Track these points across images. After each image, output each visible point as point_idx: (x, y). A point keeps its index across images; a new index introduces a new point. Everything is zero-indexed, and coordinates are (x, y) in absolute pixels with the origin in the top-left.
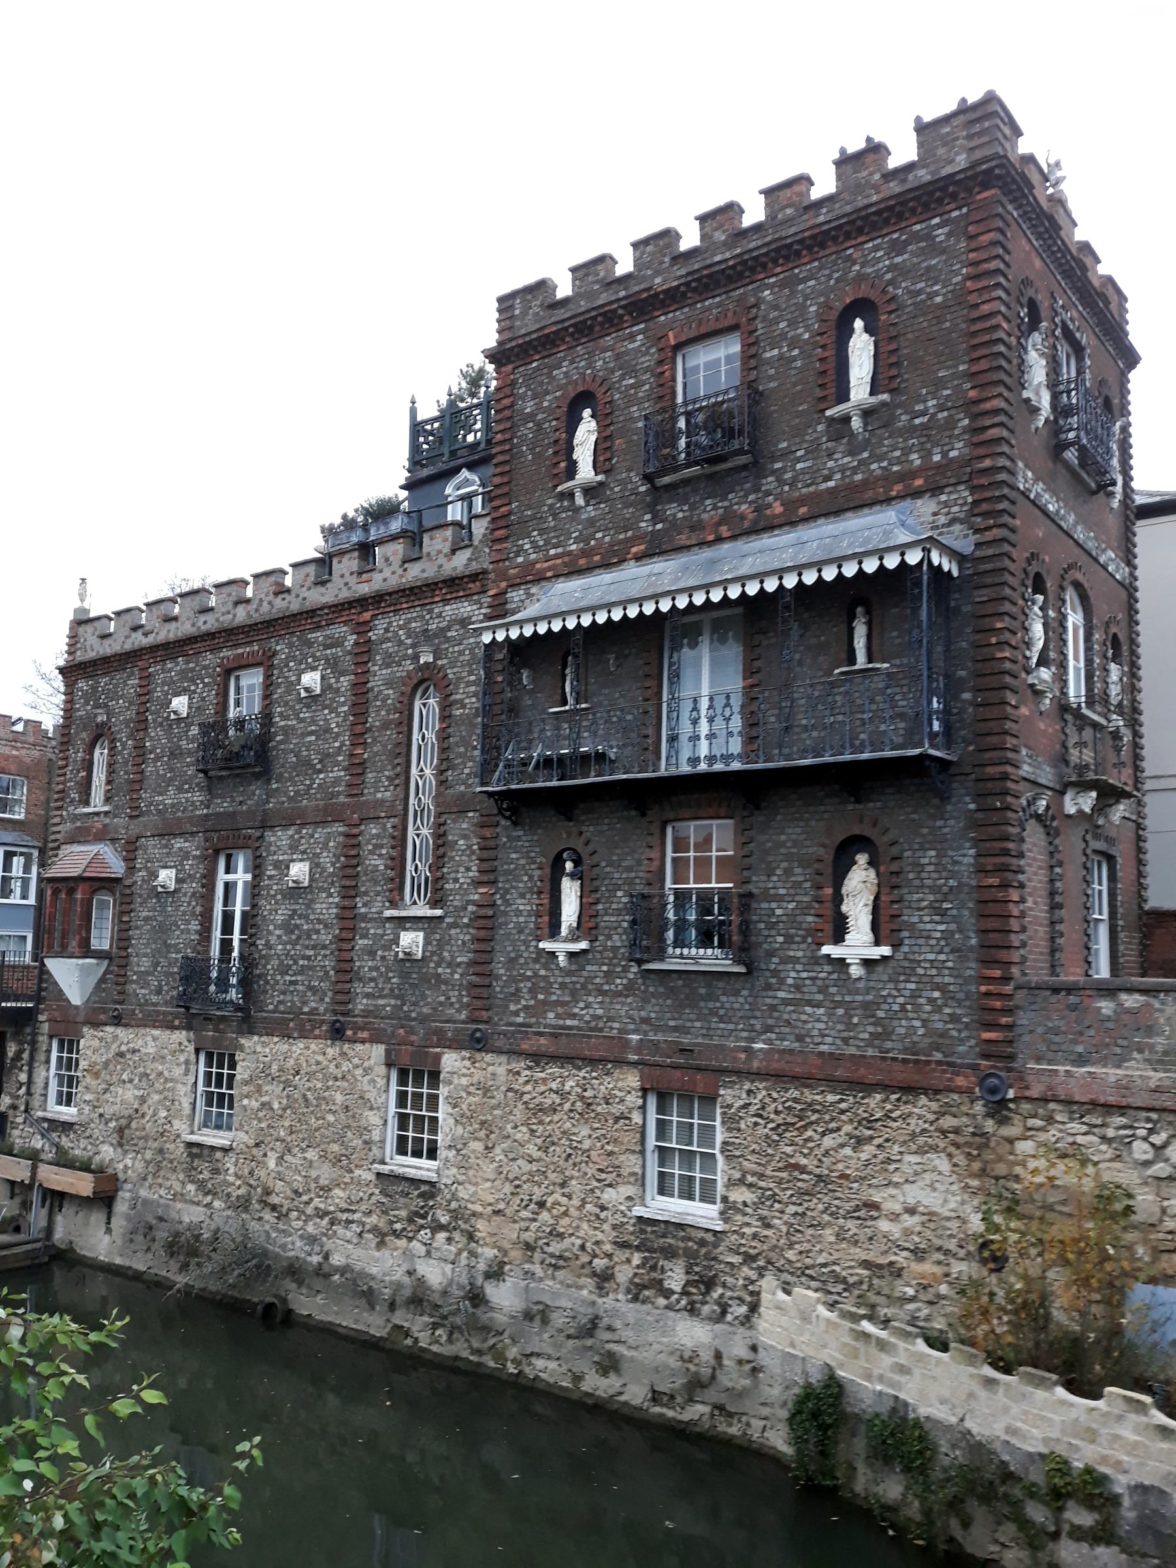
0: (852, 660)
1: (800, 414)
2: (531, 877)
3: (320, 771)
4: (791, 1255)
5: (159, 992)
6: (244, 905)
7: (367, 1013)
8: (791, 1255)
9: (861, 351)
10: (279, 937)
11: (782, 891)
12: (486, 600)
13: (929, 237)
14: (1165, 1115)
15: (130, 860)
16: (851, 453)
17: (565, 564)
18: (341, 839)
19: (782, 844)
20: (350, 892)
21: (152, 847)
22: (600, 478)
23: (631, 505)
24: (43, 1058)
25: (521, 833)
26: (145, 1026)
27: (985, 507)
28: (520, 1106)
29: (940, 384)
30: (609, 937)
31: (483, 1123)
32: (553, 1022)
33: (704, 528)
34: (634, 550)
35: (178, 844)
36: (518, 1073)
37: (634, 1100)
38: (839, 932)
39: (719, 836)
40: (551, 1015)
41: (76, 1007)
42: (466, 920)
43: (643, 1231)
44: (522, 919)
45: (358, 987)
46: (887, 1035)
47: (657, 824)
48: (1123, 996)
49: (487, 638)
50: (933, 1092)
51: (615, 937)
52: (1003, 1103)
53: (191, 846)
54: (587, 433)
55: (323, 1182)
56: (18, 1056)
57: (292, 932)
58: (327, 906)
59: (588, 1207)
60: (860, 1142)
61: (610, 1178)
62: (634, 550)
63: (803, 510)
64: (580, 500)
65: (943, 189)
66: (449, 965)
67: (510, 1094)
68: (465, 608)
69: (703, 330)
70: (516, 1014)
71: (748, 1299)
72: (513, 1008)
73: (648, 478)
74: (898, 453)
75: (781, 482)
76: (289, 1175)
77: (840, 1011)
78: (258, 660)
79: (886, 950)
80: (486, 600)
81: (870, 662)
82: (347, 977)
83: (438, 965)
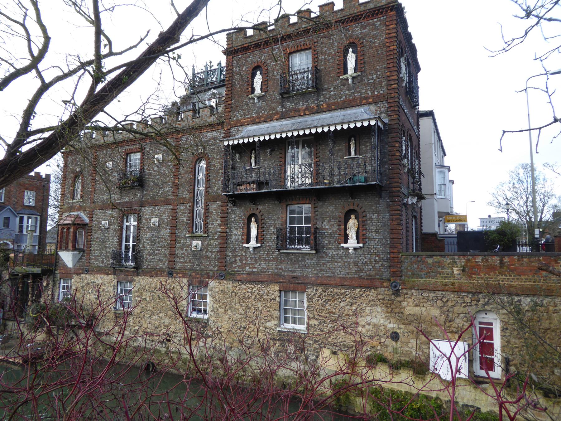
0: (350, 154)
1: (331, 77)
2: (240, 223)
3: (162, 188)
4: (330, 340)
5: (103, 262)
6: (134, 233)
7: (180, 268)
8: (330, 340)
9: (351, 59)
10: (148, 243)
11: (327, 227)
12: (223, 131)
13: (374, 25)
14: (447, 293)
15: (90, 218)
16: (349, 90)
17: (251, 121)
18: (170, 211)
19: (326, 212)
20: (174, 228)
21: (99, 212)
22: (263, 94)
23: (274, 102)
24: (58, 286)
25: (236, 209)
26: (98, 274)
27: (392, 109)
28: (237, 297)
29: (377, 70)
30: (268, 242)
31: (224, 303)
32: (249, 270)
33: (300, 111)
34: (276, 117)
35: (109, 212)
36: (236, 287)
37: (277, 294)
38: (248, 241)
39: (306, 209)
40: (248, 268)
41: (70, 268)
42: (216, 237)
43: (280, 335)
44: (236, 237)
45: (177, 260)
46: (362, 270)
47: (285, 206)
48: (434, 257)
49: (226, 143)
50: (375, 288)
51: (270, 242)
52: (398, 290)
53: (115, 213)
54: (258, 79)
55: (166, 324)
56: (48, 285)
57: (152, 242)
58: (166, 233)
59: (261, 328)
60: (352, 304)
61: (269, 319)
62: (276, 117)
63: (333, 107)
64: (256, 100)
65: (379, 10)
66: (210, 252)
67: (233, 294)
68: (215, 134)
69: (299, 48)
70: (235, 268)
71: (316, 354)
72: (234, 266)
73: (281, 94)
74: (364, 91)
75: (326, 98)
76: (153, 322)
77: (346, 264)
78: (139, 150)
79: (361, 245)
80: (223, 131)
81: (356, 155)
82: (173, 256)
83: (206, 252)
